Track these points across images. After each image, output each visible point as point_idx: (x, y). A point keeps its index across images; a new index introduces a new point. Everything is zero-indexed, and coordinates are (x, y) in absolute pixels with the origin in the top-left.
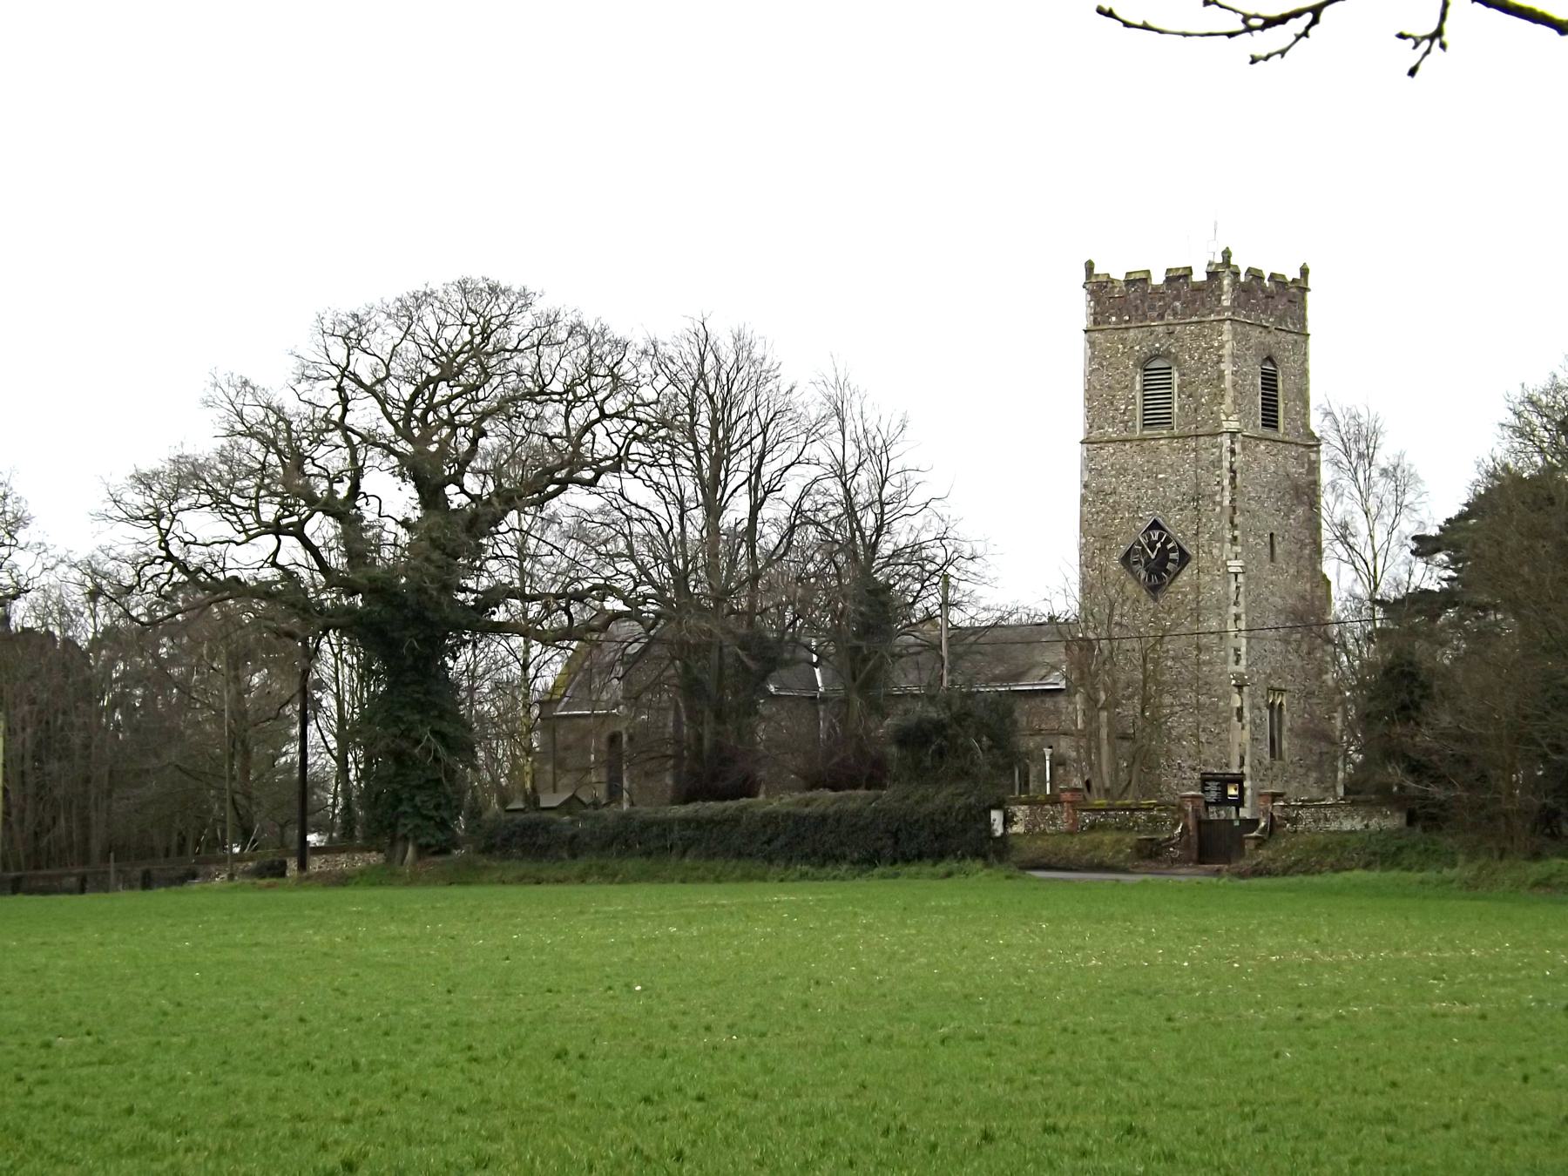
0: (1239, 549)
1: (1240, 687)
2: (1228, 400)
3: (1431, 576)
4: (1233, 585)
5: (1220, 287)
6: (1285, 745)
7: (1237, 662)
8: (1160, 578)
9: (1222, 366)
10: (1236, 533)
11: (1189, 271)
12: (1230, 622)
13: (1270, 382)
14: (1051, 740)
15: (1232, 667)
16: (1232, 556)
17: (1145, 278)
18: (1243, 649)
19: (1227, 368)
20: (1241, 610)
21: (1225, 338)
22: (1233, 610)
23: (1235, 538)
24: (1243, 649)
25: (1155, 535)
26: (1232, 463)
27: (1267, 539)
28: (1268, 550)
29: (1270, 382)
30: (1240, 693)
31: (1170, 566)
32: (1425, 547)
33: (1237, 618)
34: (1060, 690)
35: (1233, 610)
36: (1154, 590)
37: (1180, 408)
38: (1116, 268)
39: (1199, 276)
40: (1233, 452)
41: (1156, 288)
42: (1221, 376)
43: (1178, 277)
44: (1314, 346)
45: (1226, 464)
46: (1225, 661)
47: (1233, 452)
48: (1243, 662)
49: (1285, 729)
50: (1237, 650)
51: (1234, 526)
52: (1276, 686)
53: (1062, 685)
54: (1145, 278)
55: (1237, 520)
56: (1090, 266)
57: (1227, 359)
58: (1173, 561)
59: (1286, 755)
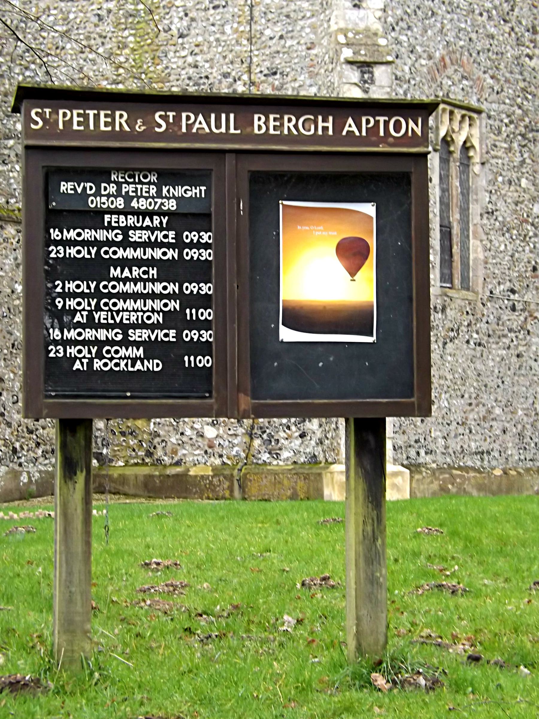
6: (476, 251)
49: (475, 209)
59: (477, 275)
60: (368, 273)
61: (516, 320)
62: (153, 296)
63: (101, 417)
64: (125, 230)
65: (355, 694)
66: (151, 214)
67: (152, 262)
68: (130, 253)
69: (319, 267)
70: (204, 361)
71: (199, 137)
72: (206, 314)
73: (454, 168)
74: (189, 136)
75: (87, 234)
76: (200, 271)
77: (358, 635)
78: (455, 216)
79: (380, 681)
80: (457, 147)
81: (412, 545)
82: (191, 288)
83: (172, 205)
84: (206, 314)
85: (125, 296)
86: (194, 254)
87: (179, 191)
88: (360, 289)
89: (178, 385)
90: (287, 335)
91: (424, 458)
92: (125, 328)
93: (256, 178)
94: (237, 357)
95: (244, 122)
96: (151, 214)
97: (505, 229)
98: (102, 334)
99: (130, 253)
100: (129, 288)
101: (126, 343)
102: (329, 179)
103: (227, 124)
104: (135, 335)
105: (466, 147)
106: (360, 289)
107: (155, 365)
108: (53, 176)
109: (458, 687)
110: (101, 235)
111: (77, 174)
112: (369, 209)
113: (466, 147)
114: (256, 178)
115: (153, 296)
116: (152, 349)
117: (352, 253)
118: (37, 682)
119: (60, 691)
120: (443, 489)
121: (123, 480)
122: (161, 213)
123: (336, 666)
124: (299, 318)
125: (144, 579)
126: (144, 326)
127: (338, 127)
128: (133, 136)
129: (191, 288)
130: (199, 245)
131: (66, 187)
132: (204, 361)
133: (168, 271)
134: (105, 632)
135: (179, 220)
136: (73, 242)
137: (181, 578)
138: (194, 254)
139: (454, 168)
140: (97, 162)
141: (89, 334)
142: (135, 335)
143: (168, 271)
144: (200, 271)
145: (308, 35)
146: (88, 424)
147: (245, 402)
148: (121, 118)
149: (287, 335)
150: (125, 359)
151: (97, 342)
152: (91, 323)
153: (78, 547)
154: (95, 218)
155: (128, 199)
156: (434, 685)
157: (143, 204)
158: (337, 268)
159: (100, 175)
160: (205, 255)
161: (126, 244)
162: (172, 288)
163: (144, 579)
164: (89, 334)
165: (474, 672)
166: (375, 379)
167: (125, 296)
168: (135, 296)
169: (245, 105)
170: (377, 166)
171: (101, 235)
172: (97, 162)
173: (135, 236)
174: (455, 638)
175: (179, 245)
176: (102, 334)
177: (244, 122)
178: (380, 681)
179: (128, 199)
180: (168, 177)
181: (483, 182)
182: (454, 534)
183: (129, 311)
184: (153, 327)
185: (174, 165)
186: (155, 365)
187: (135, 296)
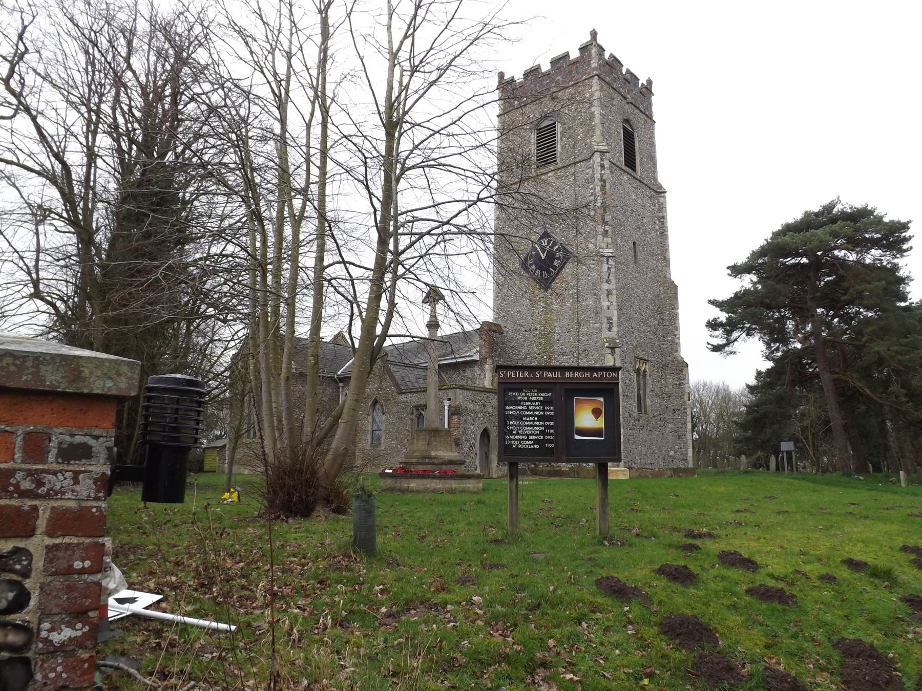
0: (609, 240)
1: (612, 349)
2: (598, 132)
3: (747, 281)
4: (605, 267)
5: (590, 56)
6: (648, 402)
7: (610, 329)
8: (549, 272)
9: (593, 109)
10: (607, 228)
11: (566, 55)
12: (603, 296)
13: (629, 138)
14: (451, 393)
15: (606, 334)
16: (604, 245)
17: (537, 69)
18: (615, 319)
19: (596, 110)
20: (612, 286)
21: (594, 89)
22: (606, 286)
23: (606, 232)
24: (615, 319)
25: (545, 242)
26: (602, 175)
27: (632, 245)
28: (632, 253)
29: (629, 138)
30: (613, 353)
31: (556, 263)
32: (737, 271)
33: (609, 293)
34: (475, 362)
35: (606, 286)
36: (546, 283)
37: (563, 147)
38: (516, 72)
39: (575, 54)
40: (602, 166)
41: (547, 74)
42: (592, 116)
43: (560, 61)
44: (657, 126)
45: (598, 176)
46: (600, 330)
47: (602, 166)
48: (615, 329)
49: (648, 390)
50: (609, 319)
51: (605, 223)
52: (641, 356)
53: (476, 357)
54: (537, 69)
55: (608, 218)
56: (501, 75)
57: (596, 103)
58: (558, 259)
59: (649, 410)
60: (602, 419)
61: (662, 423)
62: (536, 426)
63: (524, 461)
64: (528, 406)
65: (598, 547)
66: (535, 401)
67: (536, 416)
68: (529, 413)
69: (586, 418)
70: (551, 445)
71: (549, 378)
72: (552, 431)
73: (641, 377)
74: (546, 378)
75: (517, 408)
76: (549, 418)
77: (600, 529)
78: (642, 392)
79: (606, 543)
80: (642, 372)
81: (626, 495)
82: (548, 423)
83: (541, 399)
84: (552, 431)
85: (528, 426)
86: (548, 413)
87: (544, 395)
88: (600, 423)
89: (543, 452)
90: (577, 437)
91: (634, 465)
92: (528, 435)
93: (567, 390)
94: (561, 446)
95: (563, 374)
96: (535, 401)
97: (657, 396)
98: (521, 437)
99: (529, 413)
100: (529, 423)
101: (528, 439)
102: (589, 390)
103: (558, 375)
104: (531, 437)
105: (645, 371)
106: (600, 423)
107: (536, 446)
108: (507, 390)
109: (630, 545)
110: (520, 408)
111: (514, 390)
112: (602, 399)
113: (645, 371)
114: (567, 390)
115: (536, 426)
116: (536, 442)
117: (596, 413)
118: (502, 540)
119: (509, 543)
120: (640, 475)
121: (542, 471)
122: (538, 401)
123: (593, 538)
124: (581, 432)
125: (542, 505)
126: (533, 434)
127: (591, 375)
128: (529, 378)
129: (548, 423)
130: (550, 410)
131: (510, 394)
132: (551, 445)
133: (540, 418)
134: (524, 523)
135: (544, 403)
136: (512, 410)
137: (553, 505)
138: (548, 413)
139: (641, 377)
140: (519, 386)
141: (517, 437)
142: (531, 437)
143: (540, 418)
144: (549, 418)
145: (595, 340)
146: (517, 464)
147: (564, 458)
148: (526, 374)
149: (577, 437)
150: (528, 444)
151: (519, 439)
152: (518, 434)
153: (514, 500)
154: (518, 403)
155: (528, 397)
156: (623, 545)
157: (533, 398)
158: (592, 416)
159: (520, 390)
160: (552, 413)
161: (528, 410)
162: (542, 423)
163: (542, 505)
164: (517, 437)
165: (637, 540)
166: (606, 449)
167: (528, 426)
168: (531, 426)
169: (563, 369)
170: (602, 387)
171: (520, 408)
172: (519, 386)
173: (531, 408)
174: (634, 528)
175: (544, 410)
176: (521, 437)
177: (563, 374)
178: (606, 543)
179: (528, 397)
180: (540, 390)
181: (650, 382)
182: (639, 491)
183: (529, 430)
184: (536, 435)
185: (541, 387)
186: (536, 446)
187: (531, 426)
